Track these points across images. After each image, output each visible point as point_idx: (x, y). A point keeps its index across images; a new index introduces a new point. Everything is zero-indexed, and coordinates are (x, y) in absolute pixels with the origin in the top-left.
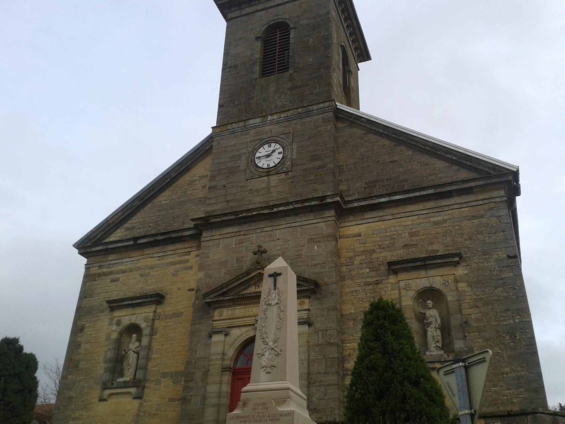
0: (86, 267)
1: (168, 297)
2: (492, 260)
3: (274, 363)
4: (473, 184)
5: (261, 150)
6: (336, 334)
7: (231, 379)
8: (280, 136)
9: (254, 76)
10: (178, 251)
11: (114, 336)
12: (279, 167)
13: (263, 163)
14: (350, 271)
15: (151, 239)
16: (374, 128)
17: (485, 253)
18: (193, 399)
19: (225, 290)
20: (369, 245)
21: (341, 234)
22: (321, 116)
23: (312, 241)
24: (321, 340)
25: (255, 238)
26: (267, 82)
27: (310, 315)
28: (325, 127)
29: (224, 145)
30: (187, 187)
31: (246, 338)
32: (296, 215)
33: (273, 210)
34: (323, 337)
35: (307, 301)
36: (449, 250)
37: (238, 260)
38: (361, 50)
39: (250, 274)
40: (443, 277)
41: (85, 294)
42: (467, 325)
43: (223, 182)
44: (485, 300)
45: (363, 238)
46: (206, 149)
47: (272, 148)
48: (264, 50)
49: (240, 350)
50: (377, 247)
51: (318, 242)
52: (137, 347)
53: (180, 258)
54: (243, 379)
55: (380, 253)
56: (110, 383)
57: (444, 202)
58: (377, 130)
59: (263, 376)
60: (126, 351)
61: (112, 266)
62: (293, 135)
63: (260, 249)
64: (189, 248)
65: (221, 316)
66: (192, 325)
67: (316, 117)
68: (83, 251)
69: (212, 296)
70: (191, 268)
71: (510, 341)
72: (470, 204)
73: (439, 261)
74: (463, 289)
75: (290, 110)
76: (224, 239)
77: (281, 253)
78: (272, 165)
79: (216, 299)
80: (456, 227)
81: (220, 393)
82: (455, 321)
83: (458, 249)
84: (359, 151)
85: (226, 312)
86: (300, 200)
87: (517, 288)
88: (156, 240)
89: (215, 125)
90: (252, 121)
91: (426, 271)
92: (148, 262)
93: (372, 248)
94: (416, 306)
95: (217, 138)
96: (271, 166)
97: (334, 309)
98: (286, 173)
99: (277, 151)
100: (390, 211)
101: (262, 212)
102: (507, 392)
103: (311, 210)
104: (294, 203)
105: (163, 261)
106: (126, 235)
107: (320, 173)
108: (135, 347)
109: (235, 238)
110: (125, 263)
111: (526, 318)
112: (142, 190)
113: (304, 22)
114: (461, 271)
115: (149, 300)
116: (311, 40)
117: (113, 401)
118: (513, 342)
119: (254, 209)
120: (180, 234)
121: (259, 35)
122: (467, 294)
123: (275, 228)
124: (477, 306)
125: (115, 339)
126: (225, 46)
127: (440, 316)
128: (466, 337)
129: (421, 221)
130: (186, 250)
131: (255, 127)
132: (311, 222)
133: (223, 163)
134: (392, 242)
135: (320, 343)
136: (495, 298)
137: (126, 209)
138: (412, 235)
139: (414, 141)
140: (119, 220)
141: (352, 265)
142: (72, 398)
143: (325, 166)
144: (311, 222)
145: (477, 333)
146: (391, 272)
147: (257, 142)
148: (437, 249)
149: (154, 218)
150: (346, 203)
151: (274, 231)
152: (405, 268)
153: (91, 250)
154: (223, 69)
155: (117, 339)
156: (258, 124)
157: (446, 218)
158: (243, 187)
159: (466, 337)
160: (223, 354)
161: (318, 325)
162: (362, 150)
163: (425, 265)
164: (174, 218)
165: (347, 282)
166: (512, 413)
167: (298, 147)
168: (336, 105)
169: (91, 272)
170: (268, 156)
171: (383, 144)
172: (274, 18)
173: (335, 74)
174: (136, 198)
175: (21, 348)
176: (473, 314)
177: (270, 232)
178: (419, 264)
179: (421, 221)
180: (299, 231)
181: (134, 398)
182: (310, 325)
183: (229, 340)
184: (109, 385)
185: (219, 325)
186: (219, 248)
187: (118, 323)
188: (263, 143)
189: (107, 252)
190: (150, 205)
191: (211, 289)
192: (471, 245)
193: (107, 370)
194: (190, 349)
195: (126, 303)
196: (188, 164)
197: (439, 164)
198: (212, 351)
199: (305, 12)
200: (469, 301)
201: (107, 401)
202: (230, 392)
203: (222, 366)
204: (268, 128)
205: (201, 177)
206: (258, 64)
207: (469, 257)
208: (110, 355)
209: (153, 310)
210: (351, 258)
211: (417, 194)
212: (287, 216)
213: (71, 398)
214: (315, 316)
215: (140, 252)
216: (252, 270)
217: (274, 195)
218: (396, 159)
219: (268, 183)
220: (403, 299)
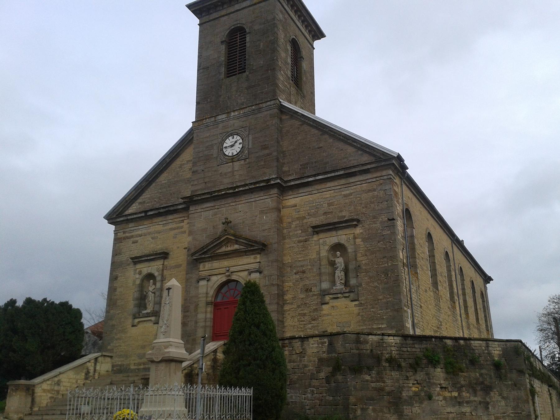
0: (115, 233)
1: (171, 253)
2: (378, 222)
3: (166, 331)
4: (369, 167)
5: (227, 141)
6: (277, 278)
7: (213, 310)
8: (240, 129)
9: (221, 76)
10: (176, 220)
11: (138, 282)
12: (240, 155)
13: (229, 152)
14: (289, 232)
15: (156, 212)
16: (307, 121)
17: (374, 217)
18: (189, 323)
19: (205, 250)
20: (302, 213)
21: (283, 205)
22: (268, 112)
23: (262, 212)
24: (267, 282)
25: (224, 211)
26: (230, 82)
27: (261, 266)
28: (271, 122)
29: (201, 137)
30: (178, 169)
31: (221, 282)
32: (252, 193)
33: (235, 190)
34: (268, 281)
35: (258, 256)
36: (352, 216)
37: (214, 227)
38: (315, 32)
39: (221, 238)
40: (347, 236)
41: (116, 253)
42: (359, 268)
43: (202, 168)
44: (371, 251)
45: (298, 207)
46: (190, 139)
47: (235, 140)
48: (229, 51)
49: (218, 290)
50: (307, 214)
51: (266, 213)
52: (154, 289)
53: (178, 225)
54: (220, 309)
55: (308, 219)
56: (138, 314)
57: (352, 180)
58: (309, 122)
59: (162, 336)
60: (147, 292)
61: (132, 231)
62: (249, 129)
63: (227, 220)
64: (182, 217)
65: (204, 268)
66: (187, 274)
67: (266, 113)
68: (111, 221)
69: (197, 255)
70: (185, 232)
71: (384, 278)
72: (368, 181)
73: (344, 225)
74: (359, 243)
75: (246, 107)
76: (205, 212)
77: (242, 222)
78: (235, 153)
79: (199, 257)
80: (358, 198)
81: (206, 319)
82: (351, 267)
83: (358, 215)
84: (296, 139)
85: (208, 265)
86: (253, 183)
87: (391, 242)
88: (159, 212)
89: (194, 121)
90: (220, 117)
91: (336, 232)
92: (156, 228)
93: (303, 215)
94: (330, 256)
95: (196, 131)
96: (234, 154)
97: (277, 261)
98: (245, 159)
99: (239, 142)
100: (317, 187)
101: (228, 192)
102: (380, 311)
103: (261, 189)
104: (249, 185)
105: (166, 228)
106: (140, 208)
107: (268, 159)
108: (153, 289)
109: (211, 211)
110: (141, 229)
111: (395, 263)
112: (147, 174)
113: (256, 27)
114: (358, 231)
115: (158, 256)
116: (262, 44)
117: (141, 326)
118: (386, 279)
119: (223, 190)
120: (175, 208)
121: (224, 39)
122: (361, 247)
123: (238, 203)
124: (366, 255)
125: (138, 284)
126: (199, 49)
127: (344, 261)
128: (358, 276)
129: (336, 194)
130: (181, 219)
131: (223, 122)
132: (261, 198)
133: (201, 152)
134: (316, 210)
135: (267, 284)
136: (378, 249)
137: (137, 188)
138: (330, 205)
139: (333, 132)
140: (133, 197)
141: (290, 228)
142: (114, 325)
143: (271, 154)
144: (261, 198)
145: (365, 273)
146: (315, 233)
147: (225, 134)
148: (345, 215)
149: (157, 194)
150: (286, 182)
151: (238, 206)
152: (323, 230)
153: (116, 221)
154: (198, 70)
155: (139, 284)
156: (225, 119)
157: (352, 191)
158: (215, 171)
159: (358, 276)
160: (207, 293)
161: (265, 272)
162: (300, 138)
163: (335, 228)
164: (171, 194)
165: (287, 241)
166: (332, 334)
167: (253, 138)
168: (280, 102)
169: (118, 236)
170: (232, 146)
171: (313, 133)
172: (234, 24)
173: (282, 72)
174: (144, 180)
175: (71, 306)
176: (363, 260)
177: (235, 206)
178: (331, 227)
179: (336, 194)
180: (254, 205)
181: (154, 323)
182: (260, 273)
183: (210, 283)
184: (137, 315)
185: (204, 274)
186: (201, 219)
187: (140, 273)
188: (229, 135)
189: (128, 221)
190: (154, 184)
191: (197, 249)
192: (366, 211)
193: (135, 306)
194: (186, 290)
195: (143, 259)
196: (177, 152)
197: (350, 150)
198: (199, 292)
199: (257, 17)
200: (362, 251)
201: (137, 326)
202: (212, 317)
203: (206, 301)
204: (231, 122)
205: (188, 161)
206: (224, 65)
207: (364, 221)
208: (137, 295)
209: (162, 263)
210: (289, 223)
211: (333, 174)
212: (245, 194)
213: (113, 326)
214: (264, 266)
215: (150, 221)
216: (222, 236)
217: (237, 177)
218: (322, 146)
219: (233, 167)
220: (321, 251)
